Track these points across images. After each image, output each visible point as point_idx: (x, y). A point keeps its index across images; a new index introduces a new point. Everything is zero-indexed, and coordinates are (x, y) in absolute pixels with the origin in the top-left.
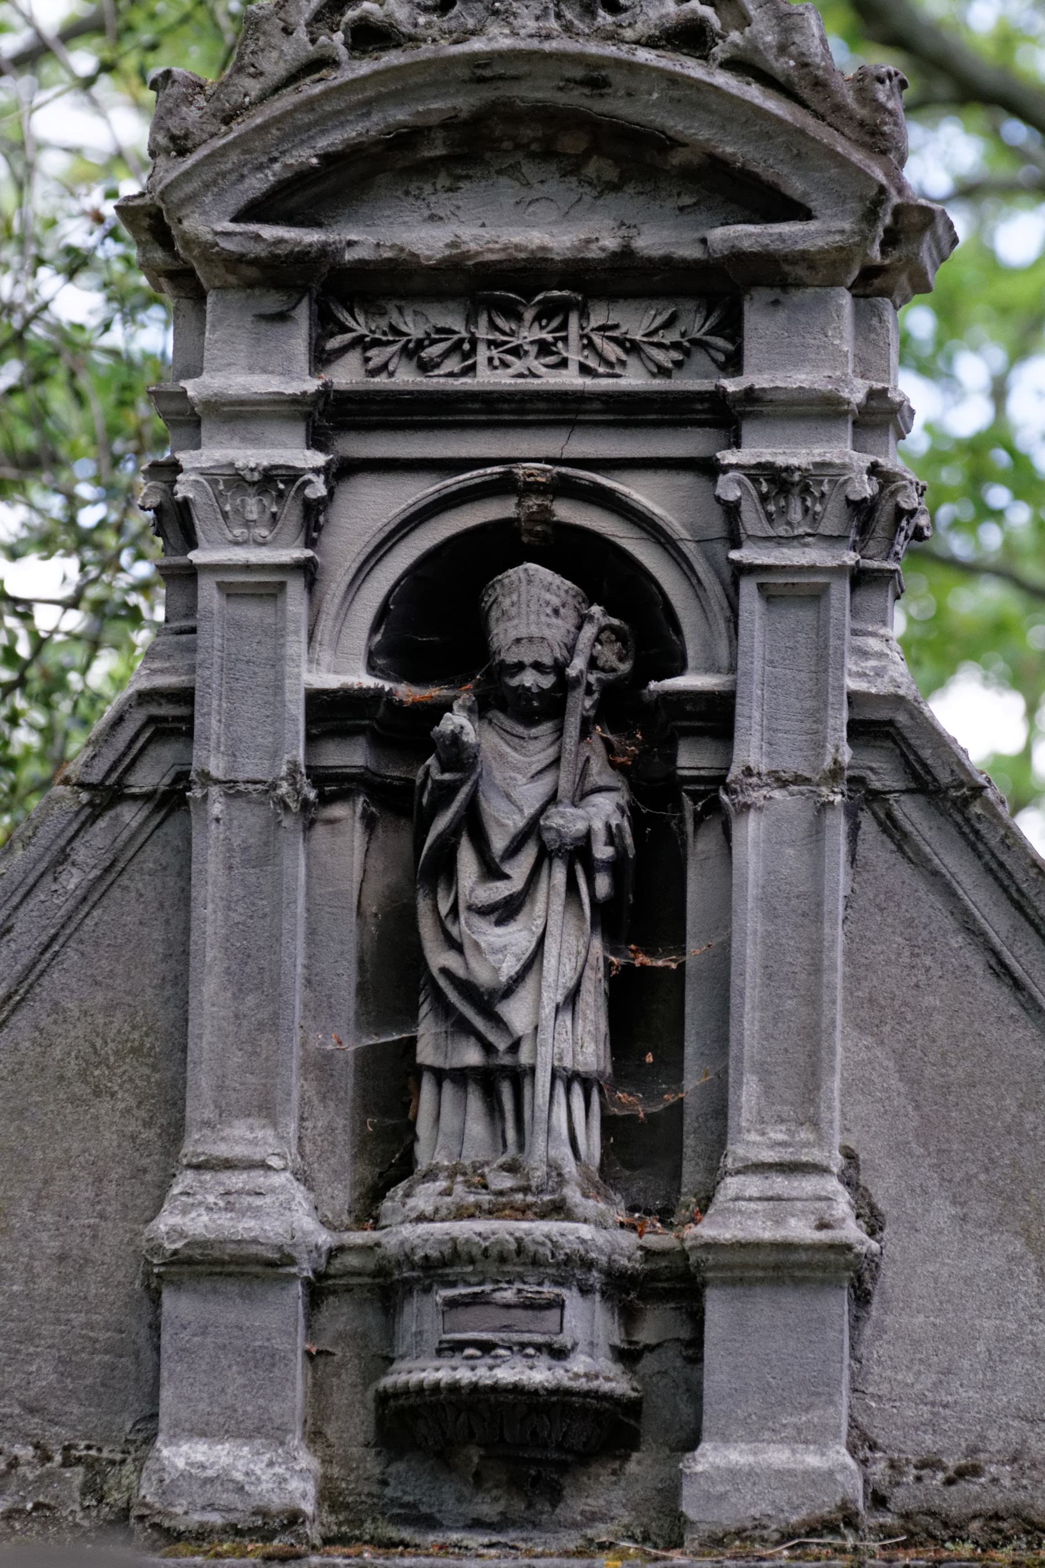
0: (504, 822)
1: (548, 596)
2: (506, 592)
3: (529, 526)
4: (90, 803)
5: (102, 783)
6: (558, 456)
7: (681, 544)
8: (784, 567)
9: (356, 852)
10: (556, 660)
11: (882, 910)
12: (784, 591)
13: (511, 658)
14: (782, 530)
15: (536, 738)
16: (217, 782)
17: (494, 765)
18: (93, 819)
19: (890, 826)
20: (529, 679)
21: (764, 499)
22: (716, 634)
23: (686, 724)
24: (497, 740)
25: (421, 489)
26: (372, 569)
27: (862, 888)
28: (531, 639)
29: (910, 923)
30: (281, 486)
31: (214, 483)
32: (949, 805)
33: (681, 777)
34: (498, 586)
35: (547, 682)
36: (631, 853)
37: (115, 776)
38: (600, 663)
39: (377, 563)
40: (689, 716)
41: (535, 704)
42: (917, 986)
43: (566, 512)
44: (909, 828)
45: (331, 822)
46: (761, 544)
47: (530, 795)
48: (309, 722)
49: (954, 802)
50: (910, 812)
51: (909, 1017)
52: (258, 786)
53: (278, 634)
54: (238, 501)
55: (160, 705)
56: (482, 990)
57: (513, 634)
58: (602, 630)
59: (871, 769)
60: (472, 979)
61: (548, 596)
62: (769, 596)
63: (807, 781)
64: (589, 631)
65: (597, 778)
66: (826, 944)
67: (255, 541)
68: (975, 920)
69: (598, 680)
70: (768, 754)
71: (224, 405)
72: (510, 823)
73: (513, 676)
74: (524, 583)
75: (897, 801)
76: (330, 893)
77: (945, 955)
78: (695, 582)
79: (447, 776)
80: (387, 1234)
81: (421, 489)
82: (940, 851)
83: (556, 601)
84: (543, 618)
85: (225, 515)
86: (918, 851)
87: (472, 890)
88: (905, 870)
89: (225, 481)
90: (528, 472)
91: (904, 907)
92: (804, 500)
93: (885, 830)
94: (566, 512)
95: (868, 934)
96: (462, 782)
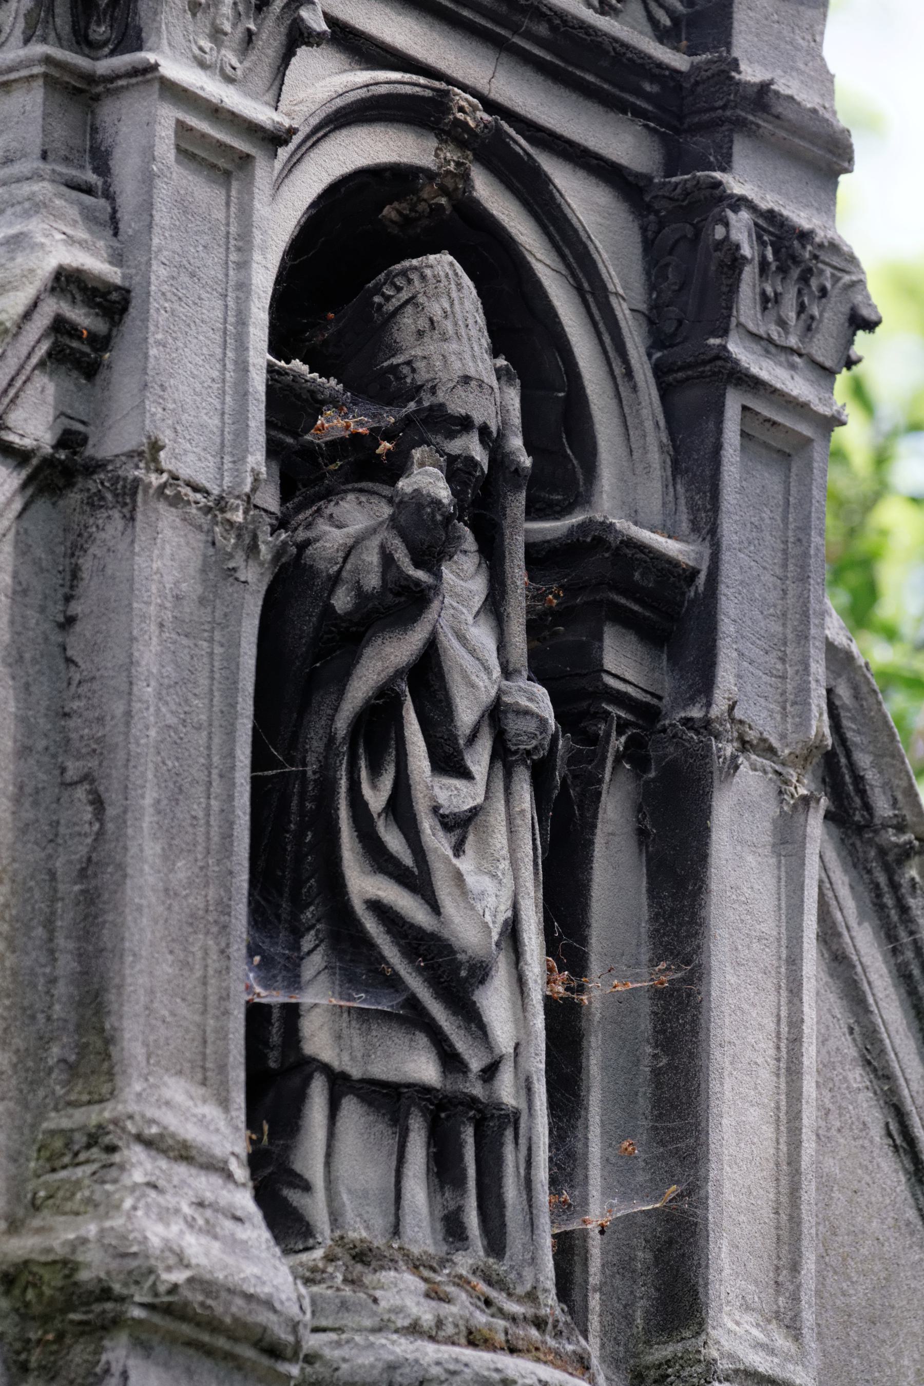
7: (614, 301)
8: (775, 391)
22: (639, 468)
23: (623, 601)
32: (873, 853)
33: (606, 686)
40: (630, 591)
43: (486, 191)
49: (882, 852)
52: (199, 496)
55: (74, 302)
56: (461, 957)
60: (446, 934)
68: (883, 1051)
78: (619, 370)
80: (338, 1344)
94: (486, 191)
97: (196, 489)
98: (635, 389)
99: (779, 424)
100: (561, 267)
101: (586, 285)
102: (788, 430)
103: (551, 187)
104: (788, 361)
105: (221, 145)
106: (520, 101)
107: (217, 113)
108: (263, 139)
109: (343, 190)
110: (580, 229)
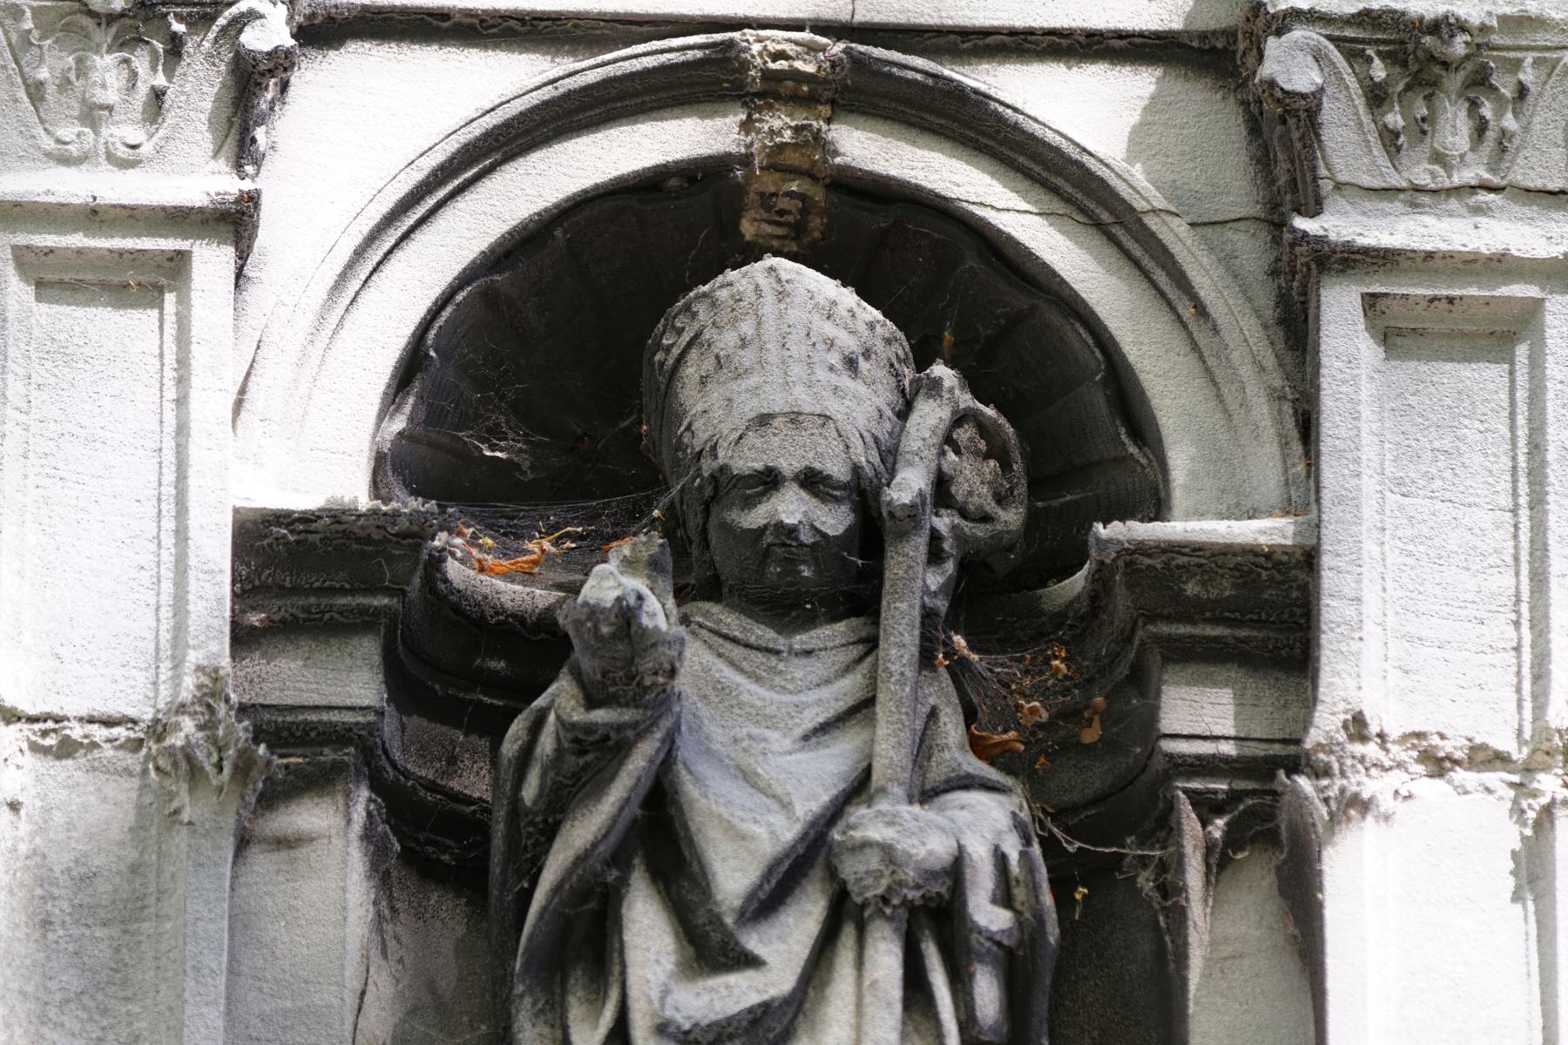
0: (739, 840)
1: (829, 329)
2: (724, 316)
3: (769, 183)
6: (844, 16)
7: (1152, 222)
8: (1430, 255)
9: (352, 917)
10: (856, 469)
13: (747, 461)
14: (1422, 173)
15: (808, 653)
17: (704, 711)
20: (791, 507)
21: (1377, 97)
23: (1183, 629)
24: (708, 658)
25: (511, 79)
28: (795, 418)
30: (178, 27)
33: (1171, 756)
34: (701, 309)
35: (834, 520)
40: (1191, 611)
43: (865, 148)
45: (284, 843)
46: (1368, 205)
47: (811, 779)
48: (246, 591)
52: (117, 731)
57: (750, 407)
58: (960, 419)
61: (829, 329)
62: (1395, 333)
63: (1499, 760)
64: (930, 416)
67: (111, 158)
72: (761, 831)
73: (749, 503)
74: (769, 298)
76: (286, 1013)
78: (1187, 312)
79: (600, 715)
81: (511, 79)
83: (850, 343)
84: (822, 374)
85: (36, 92)
87: (665, 992)
90: (772, 47)
92: (1474, 105)
94: (865, 148)
97: (108, 723)
98: (1215, 330)
100: (1058, 206)
101: (1105, 217)
103: (993, 105)
109: (558, 233)
110: (1064, 145)
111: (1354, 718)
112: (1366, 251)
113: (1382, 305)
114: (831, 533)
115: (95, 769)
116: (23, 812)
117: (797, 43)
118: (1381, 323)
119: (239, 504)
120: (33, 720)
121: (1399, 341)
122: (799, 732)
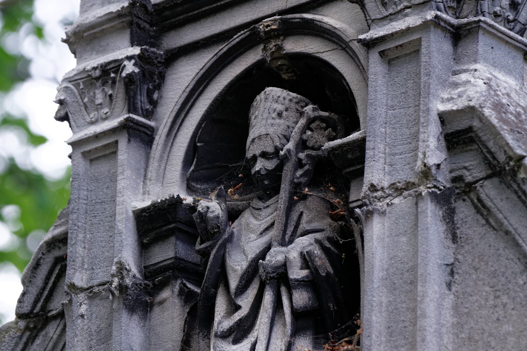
4: (27, 328)
5: (31, 312)
8: (392, 34)
11: (476, 269)
12: (397, 53)
16: (82, 290)
18: (32, 340)
19: (481, 209)
26: (183, 121)
27: (465, 257)
29: (494, 275)
31: (77, 86)
35: (270, 165)
36: (332, 272)
37: (40, 305)
38: (310, 144)
39: (186, 116)
41: (266, 182)
42: (498, 319)
43: (294, 46)
44: (489, 204)
45: (161, 303)
50: (490, 192)
51: (493, 344)
53: (114, 179)
54: (92, 94)
59: (465, 168)
62: (389, 59)
65: (305, 225)
66: (419, 299)
69: (308, 156)
70: (390, 173)
71: (84, 32)
72: (239, 268)
75: (481, 187)
77: (515, 292)
82: (508, 214)
83: (280, 107)
84: (270, 121)
86: (497, 220)
88: (491, 236)
89: (83, 83)
91: (490, 263)
93: (478, 211)
94: (294, 46)
95: (469, 290)
96: (212, 247)
99: (403, 44)
100: (335, 46)
102: (410, 43)
104: (402, 15)
105: (105, 146)
106: (197, 36)
107: (97, 137)
108: (120, 130)
111: (371, 186)
112: (377, 39)
113: (386, 53)
114: (270, 169)
115: (102, 299)
116: (85, 317)
117: (272, 21)
118: (387, 59)
119: (133, 209)
120: (88, 289)
121: (393, 62)
122: (259, 232)
